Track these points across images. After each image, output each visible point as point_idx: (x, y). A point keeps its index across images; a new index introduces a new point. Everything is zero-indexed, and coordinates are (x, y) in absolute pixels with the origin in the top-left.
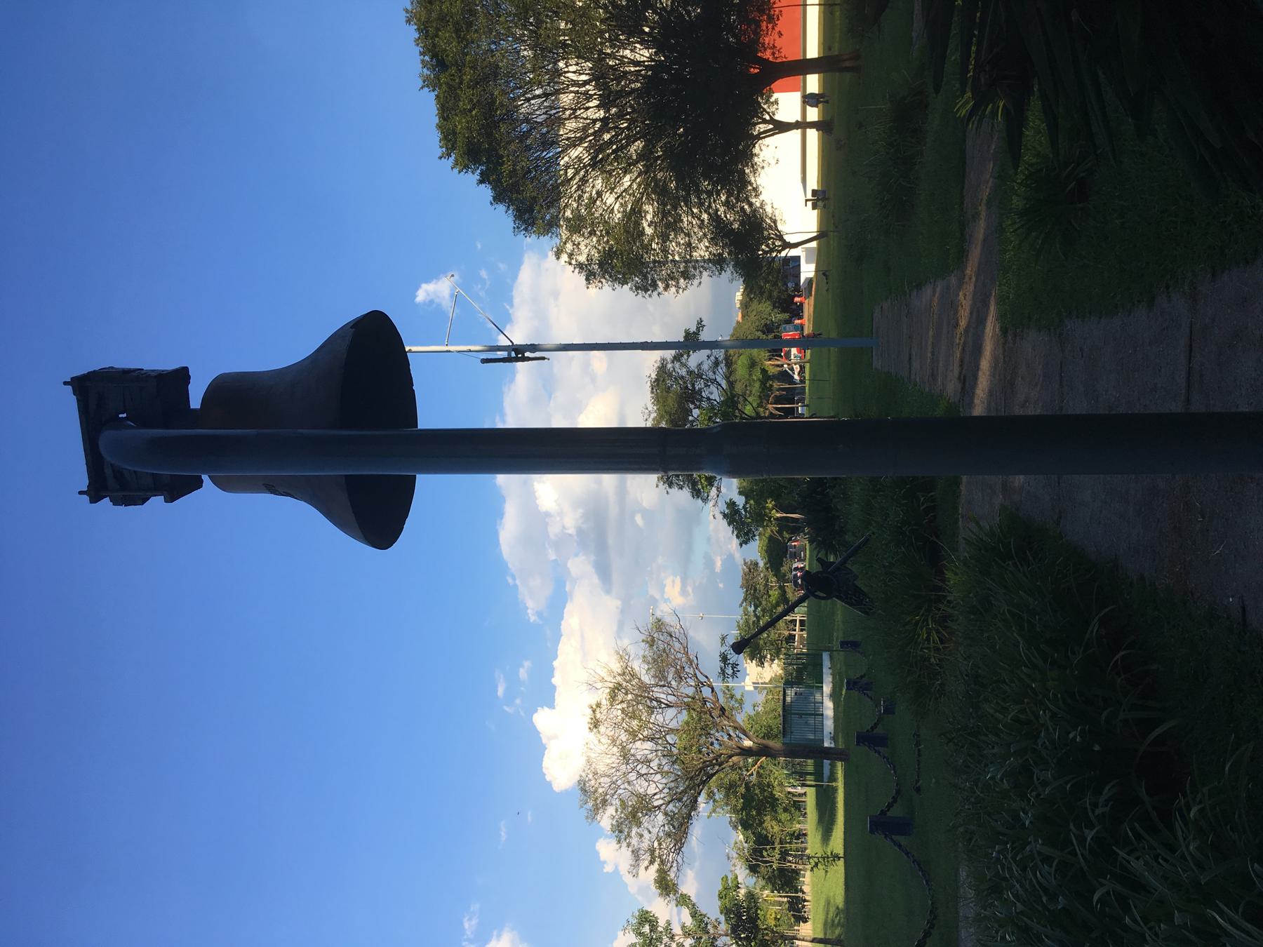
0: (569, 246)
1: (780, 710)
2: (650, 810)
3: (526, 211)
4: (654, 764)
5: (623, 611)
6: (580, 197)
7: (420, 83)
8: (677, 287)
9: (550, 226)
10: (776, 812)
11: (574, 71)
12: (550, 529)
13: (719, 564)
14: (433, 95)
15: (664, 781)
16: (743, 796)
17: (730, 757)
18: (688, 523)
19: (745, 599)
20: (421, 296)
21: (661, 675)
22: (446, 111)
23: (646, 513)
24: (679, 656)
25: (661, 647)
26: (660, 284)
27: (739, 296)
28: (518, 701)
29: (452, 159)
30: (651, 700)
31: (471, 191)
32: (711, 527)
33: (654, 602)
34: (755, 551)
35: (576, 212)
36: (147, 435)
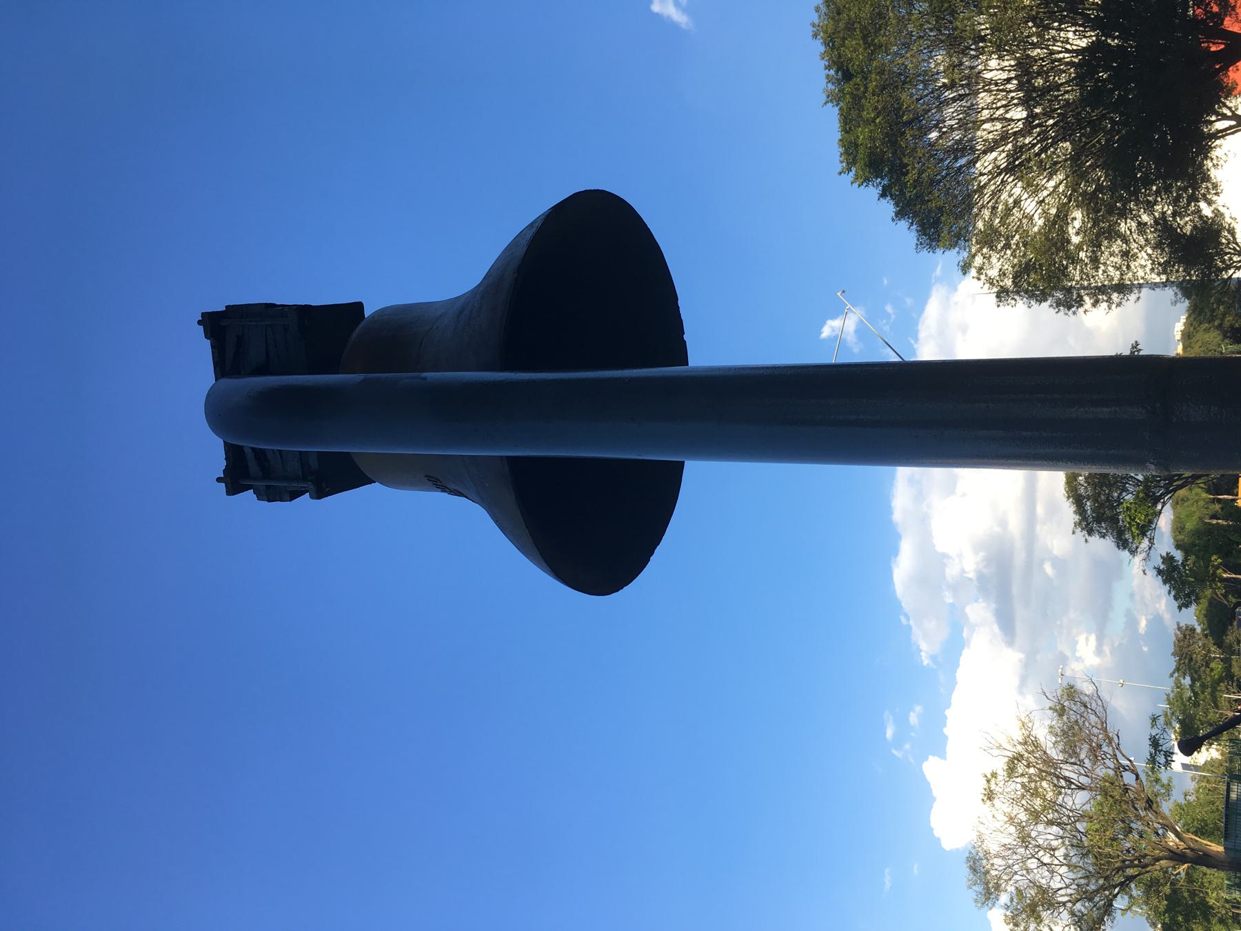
0: (978, 260)
1: (1222, 807)
2: (1051, 905)
3: (932, 226)
4: (1060, 853)
5: (1028, 666)
6: (994, 208)
7: (824, 98)
8: (1109, 301)
9: (959, 238)
10: (1209, 921)
11: (996, 68)
12: (948, 571)
13: (1143, 623)
14: (836, 110)
15: (1071, 875)
16: (1167, 897)
17: (1158, 859)
18: (1105, 577)
19: (1178, 669)
20: (826, 332)
21: (1071, 751)
22: (848, 123)
23: (1059, 563)
24: (1095, 731)
25: (1073, 718)
26: (1086, 298)
27: (1179, 326)
28: (907, 746)
29: (852, 174)
30: (1058, 777)
31: (871, 207)
32: (1135, 583)
33: (1063, 659)
34: (1191, 617)
35: (989, 225)
36: (307, 395)
